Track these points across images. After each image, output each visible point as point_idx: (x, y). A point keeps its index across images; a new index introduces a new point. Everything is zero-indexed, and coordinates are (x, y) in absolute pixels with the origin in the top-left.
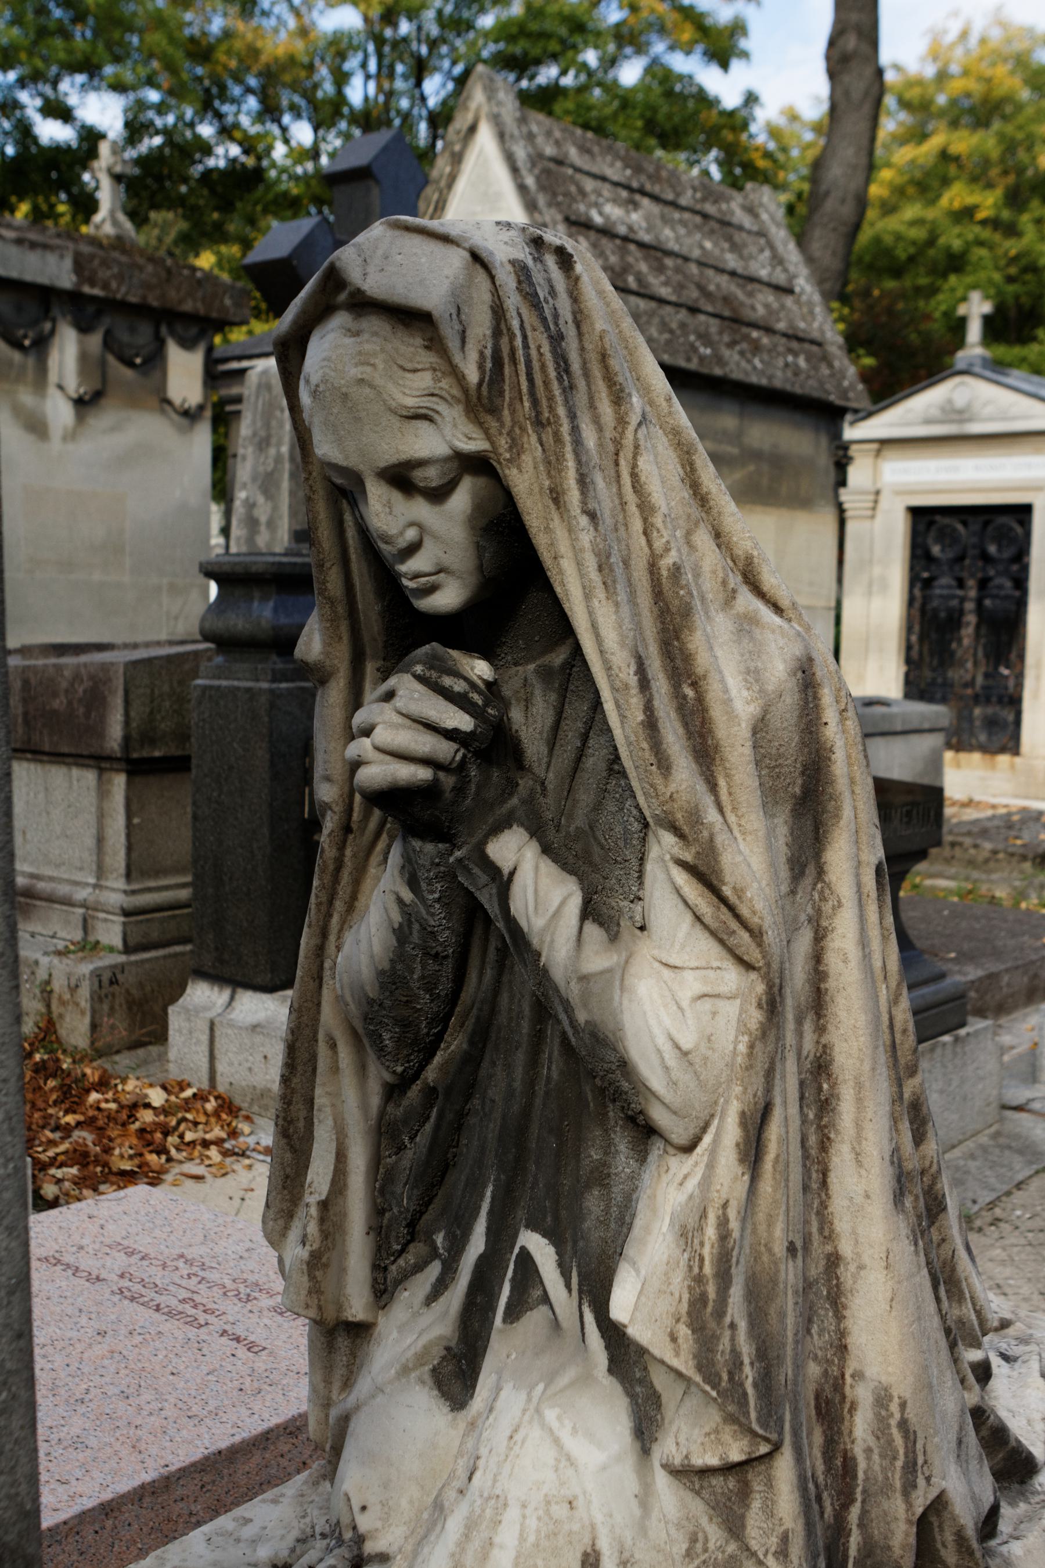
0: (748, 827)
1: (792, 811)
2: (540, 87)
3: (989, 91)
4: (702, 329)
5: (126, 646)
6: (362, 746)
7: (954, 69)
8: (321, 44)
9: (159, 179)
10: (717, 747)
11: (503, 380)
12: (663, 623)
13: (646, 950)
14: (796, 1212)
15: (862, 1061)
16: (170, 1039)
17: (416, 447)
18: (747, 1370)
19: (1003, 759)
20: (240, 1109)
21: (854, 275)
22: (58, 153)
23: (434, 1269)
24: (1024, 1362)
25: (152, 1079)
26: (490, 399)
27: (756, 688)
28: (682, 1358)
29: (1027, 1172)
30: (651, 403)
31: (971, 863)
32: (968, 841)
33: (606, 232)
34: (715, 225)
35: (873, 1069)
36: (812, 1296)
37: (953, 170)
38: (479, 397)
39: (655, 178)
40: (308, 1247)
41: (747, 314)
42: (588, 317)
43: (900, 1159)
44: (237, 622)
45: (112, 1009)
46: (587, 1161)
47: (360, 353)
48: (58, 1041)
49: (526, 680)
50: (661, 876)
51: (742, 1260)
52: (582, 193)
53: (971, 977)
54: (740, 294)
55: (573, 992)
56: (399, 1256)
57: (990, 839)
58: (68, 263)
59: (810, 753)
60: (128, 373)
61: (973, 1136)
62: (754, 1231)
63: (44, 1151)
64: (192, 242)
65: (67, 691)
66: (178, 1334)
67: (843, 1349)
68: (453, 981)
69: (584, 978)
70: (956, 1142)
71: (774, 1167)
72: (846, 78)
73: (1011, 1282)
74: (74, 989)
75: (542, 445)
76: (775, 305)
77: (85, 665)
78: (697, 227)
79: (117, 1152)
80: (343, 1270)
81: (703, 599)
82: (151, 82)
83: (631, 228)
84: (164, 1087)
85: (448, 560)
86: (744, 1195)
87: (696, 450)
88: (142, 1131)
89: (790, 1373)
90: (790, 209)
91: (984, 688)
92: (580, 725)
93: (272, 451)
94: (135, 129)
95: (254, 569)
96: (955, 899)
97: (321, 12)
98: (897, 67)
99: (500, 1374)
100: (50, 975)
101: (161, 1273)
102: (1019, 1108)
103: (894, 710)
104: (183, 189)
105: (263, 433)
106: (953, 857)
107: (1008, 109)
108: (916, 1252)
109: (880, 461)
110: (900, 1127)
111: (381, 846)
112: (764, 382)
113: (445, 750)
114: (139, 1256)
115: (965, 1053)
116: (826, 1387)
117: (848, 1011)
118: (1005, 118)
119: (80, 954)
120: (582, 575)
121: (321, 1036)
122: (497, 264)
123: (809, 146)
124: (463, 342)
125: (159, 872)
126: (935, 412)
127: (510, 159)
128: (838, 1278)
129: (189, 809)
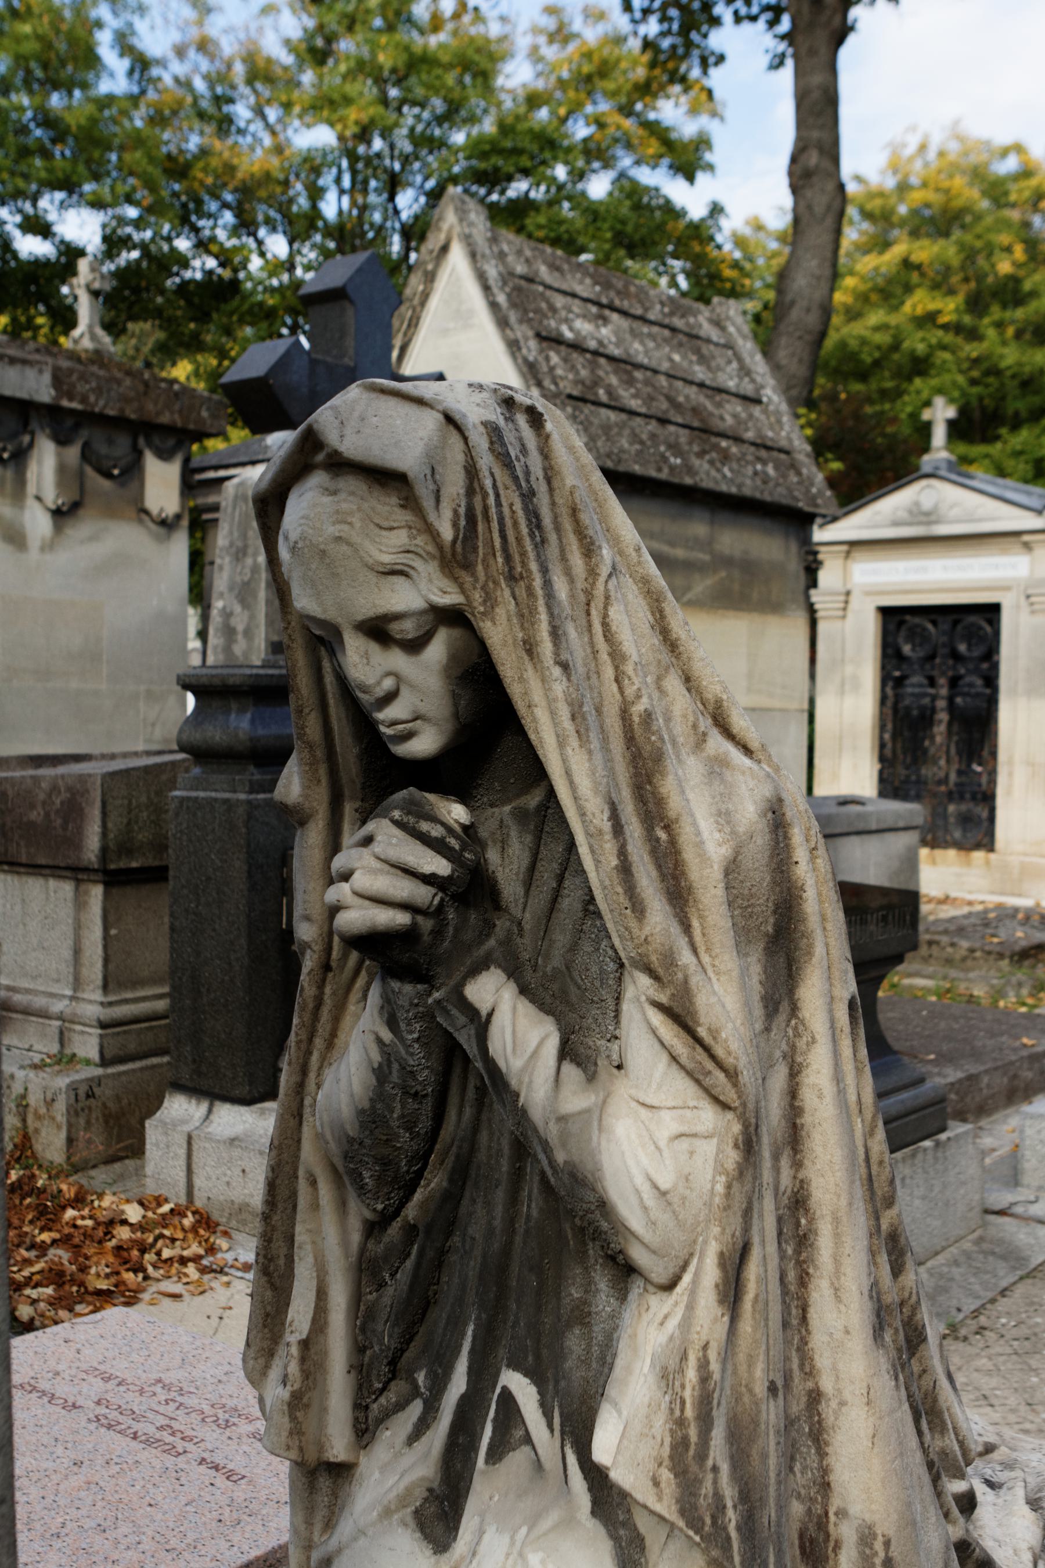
0: (722, 967)
1: (765, 949)
2: (510, 201)
3: (949, 200)
4: (672, 439)
5: (103, 757)
6: (341, 891)
7: (914, 180)
8: (297, 160)
9: (136, 291)
10: (690, 889)
11: (477, 537)
12: (635, 767)
13: (623, 1089)
14: (776, 1351)
15: (839, 1196)
16: (148, 1153)
17: (393, 601)
18: (731, 1513)
19: (979, 855)
20: (218, 1224)
21: (821, 380)
22: (38, 264)
23: (416, 1408)
24: (1009, 1489)
25: (130, 1195)
26: (465, 557)
27: (727, 830)
28: (665, 1502)
29: (1011, 1279)
30: (621, 553)
31: (949, 962)
32: (945, 939)
33: (577, 347)
34: (684, 339)
35: (850, 1204)
36: (794, 1434)
37: (915, 277)
38: (454, 553)
39: (623, 294)
40: (289, 1388)
41: (717, 425)
42: (559, 473)
43: (878, 1293)
44: (215, 734)
45: (88, 1122)
46: (567, 1300)
47: (337, 512)
48: (34, 1156)
49: (502, 821)
50: (637, 1016)
51: (723, 1402)
52: (553, 309)
53: (950, 1079)
54: (709, 406)
55: (552, 1132)
56: (381, 1394)
57: (967, 938)
58: (47, 378)
59: (781, 892)
60: (106, 484)
61: (956, 1242)
62: (735, 1372)
63: (20, 1270)
64: (169, 352)
65: (44, 803)
66: (157, 1463)
67: (825, 1486)
68: (433, 1119)
69: (562, 1119)
70: (939, 1248)
71: (753, 1306)
72: (809, 193)
73: (998, 1392)
74: (50, 1103)
75: (515, 598)
76: (744, 415)
77: (63, 777)
78: (666, 340)
79: (93, 1271)
80: (324, 1410)
81: (674, 742)
82: (129, 200)
83: (600, 343)
84: (141, 1203)
85: (424, 708)
86: (724, 1337)
87: (665, 598)
88: (119, 1248)
89: (773, 1515)
90: (757, 319)
91: (957, 785)
92: (555, 866)
93: (249, 561)
94: (113, 243)
95: (231, 681)
96: (934, 999)
97: (296, 131)
98: (858, 179)
99: (482, 1515)
100: (26, 1089)
101: (138, 1400)
102: (1001, 1213)
103: (869, 808)
104: (159, 300)
105: (239, 544)
106: (930, 956)
107: (968, 219)
108: (897, 1387)
109: (849, 562)
110: (879, 1260)
111: (360, 982)
112: (734, 490)
113: (423, 894)
114: (116, 1381)
115: (946, 1158)
116: (810, 1525)
117: (825, 1146)
118: (963, 227)
119: (57, 1068)
120: (556, 724)
121: (301, 1173)
122: (470, 426)
123: (775, 255)
124: (438, 500)
125: (136, 983)
126: (903, 515)
127: (482, 277)
128: (819, 1414)
129: (166, 920)
